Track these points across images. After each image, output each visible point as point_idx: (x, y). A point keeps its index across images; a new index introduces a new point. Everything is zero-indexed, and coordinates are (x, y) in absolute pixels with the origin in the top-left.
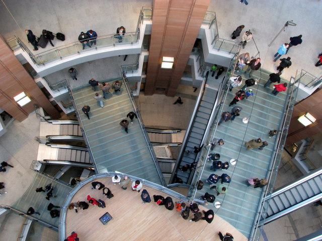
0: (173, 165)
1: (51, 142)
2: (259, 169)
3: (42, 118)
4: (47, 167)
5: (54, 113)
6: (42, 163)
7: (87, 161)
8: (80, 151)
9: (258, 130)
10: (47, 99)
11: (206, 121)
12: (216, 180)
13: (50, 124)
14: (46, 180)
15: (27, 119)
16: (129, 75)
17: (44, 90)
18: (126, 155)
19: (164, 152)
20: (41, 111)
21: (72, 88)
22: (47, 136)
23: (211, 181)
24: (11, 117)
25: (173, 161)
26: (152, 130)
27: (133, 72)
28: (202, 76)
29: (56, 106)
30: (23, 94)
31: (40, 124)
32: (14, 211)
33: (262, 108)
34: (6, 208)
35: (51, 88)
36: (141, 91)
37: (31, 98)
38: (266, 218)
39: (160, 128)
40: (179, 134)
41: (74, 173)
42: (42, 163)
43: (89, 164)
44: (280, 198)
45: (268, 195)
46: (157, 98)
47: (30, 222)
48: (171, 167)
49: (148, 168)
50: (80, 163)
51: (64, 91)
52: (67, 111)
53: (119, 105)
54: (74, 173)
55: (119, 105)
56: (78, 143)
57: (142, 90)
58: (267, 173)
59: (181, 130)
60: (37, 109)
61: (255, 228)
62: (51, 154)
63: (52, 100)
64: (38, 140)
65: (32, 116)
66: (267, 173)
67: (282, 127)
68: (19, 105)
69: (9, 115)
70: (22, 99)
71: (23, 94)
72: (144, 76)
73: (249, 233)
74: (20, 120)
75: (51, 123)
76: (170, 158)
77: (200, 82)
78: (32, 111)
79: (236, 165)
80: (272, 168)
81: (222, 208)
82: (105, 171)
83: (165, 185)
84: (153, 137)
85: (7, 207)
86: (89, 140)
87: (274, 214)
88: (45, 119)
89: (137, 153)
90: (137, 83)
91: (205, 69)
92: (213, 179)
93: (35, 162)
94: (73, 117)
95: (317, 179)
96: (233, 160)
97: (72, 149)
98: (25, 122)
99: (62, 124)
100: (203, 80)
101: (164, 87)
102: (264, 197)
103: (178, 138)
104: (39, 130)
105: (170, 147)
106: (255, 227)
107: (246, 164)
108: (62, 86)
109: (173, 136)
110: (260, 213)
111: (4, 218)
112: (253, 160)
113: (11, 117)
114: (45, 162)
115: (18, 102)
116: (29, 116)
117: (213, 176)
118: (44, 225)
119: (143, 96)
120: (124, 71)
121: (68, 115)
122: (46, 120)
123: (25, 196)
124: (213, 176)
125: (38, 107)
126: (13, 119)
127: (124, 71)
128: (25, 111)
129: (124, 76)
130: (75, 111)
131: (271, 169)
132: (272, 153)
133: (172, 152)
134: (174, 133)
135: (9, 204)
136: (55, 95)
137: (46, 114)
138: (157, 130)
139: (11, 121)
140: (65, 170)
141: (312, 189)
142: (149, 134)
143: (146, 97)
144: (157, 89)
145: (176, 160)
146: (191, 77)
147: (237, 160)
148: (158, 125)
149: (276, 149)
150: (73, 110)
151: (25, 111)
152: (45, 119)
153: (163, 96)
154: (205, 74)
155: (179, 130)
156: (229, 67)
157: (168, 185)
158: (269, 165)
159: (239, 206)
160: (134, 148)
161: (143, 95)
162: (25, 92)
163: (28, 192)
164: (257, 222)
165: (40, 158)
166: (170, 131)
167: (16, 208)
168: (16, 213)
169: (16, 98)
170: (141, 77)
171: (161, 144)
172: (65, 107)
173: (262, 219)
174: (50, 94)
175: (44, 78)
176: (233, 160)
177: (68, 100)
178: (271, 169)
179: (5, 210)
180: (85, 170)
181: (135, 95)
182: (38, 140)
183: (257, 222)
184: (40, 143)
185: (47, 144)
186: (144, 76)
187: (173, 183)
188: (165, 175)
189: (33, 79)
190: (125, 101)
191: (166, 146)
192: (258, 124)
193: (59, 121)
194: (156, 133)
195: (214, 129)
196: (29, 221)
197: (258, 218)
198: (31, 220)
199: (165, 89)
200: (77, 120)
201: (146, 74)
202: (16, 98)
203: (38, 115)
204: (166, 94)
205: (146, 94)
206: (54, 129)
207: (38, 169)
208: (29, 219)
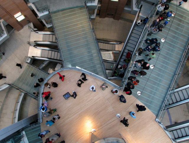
0: (115, 64)
1: (37, 45)
2: (163, 85)
3: (32, 29)
4: (35, 61)
5: (40, 26)
6: (31, 58)
7: (58, 59)
8: (57, 52)
9: (171, 47)
10: (35, 17)
11: (140, 33)
12: (150, 49)
13: (37, 34)
14: (33, 69)
15: (22, 30)
16: (89, 4)
17: (33, 11)
18: (84, 57)
19: (108, 56)
20: (31, 25)
21: (51, 10)
22: (35, 41)
23: (147, 50)
24: (13, 28)
25: (115, 62)
26: (103, 41)
27: (91, 2)
28: (138, 8)
29: (42, 22)
30: (20, 14)
31: (30, 33)
32: (14, 87)
33: (175, 33)
34: (8, 84)
35: (38, 10)
36: (97, 15)
37: (25, 16)
38: (169, 105)
39: (108, 40)
40: (120, 45)
41: (53, 64)
42: (31, 58)
43: (60, 60)
44: (178, 93)
45: (172, 90)
46: (108, 20)
47: (23, 94)
48: (113, 66)
49: (97, 66)
50: (57, 60)
51: (46, 13)
52: (48, 26)
53: (81, 23)
54: (53, 64)
55: (81, 23)
56: (54, 47)
57: (98, 14)
58: (174, 76)
59: (122, 43)
60: (29, 23)
61: (161, 111)
62: (36, 53)
63: (39, 18)
64: (29, 43)
65: (26, 28)
66: (174, 76)
67: (188, 47)
68: (17, 21)
69: (11, 27)
70: (20, 17)
71: (20, 14)
72: (99, 5)
73: (157, 113)
74: (18, 30)
75: (38, 33)
76: (113, 60)
77: (136, 12)
78: (26, 25)
79: (153, 69)
80: (177, 73)
81: (142, 96)
82: (70, 66)
83: (107, 78)
84: (102, 45)
85: (9, 84)
86: (62, 45)
87: (173, 103)
88: (34, 30)
89: (92, 55)
90: (94, 10)
91: (140, 3)
92: (149, 49)
93: (27, 57)
94: (52, 30)
95: (186, 129)
96: (152, 65)
97: (49, 50)
98: (22, 31)
99: (44, 34)
100: (138, 10)
101: (112, 13)
102: (170, 91)
103: (119, 48)
104: (30, 37)
105: (113, 53)
106: (168, 94)
107: (160, 69)
108: (44, 10)
109: (117, 46)
110: (167, 98)
111: (7, 91)
112: (164, 71)
113: (13, 28)
114: (33, 58)
115: (17, 19)
116: (24, 28)
117: (149, 47)
118: (32, 97)
119: (98, 19)
120: (85, 2)
121: (49, 28)
122: (35, 31)
123: (20, 78)
124: (149, 47)
125: (30, 22)
126: (14, 29)
127: (85, 2)
128: (21, 24)
129: (86, 5)
130: (52, 26)
131: (171, 87)
132: (184, 50)
133: (115, 57)
134: (117, 44)
135: (11, 82)
136: (40, 15)
137: (35, 27)
138: (106, 41)
139: (12, 31)
140: (46, 63)
141: (181, 132)
142: (99, 43)
143: (101, 19)
144: (108, 14)
145: (116, 62)
146: (131, 8)
147: (154, 66)
148: (107, 38)
149: (181, 61)
150: (51, 25)
151: (21, 24)
152: (34, 30)
153: (112, 19)
154: (140, 7)
155: (121, 42)
156: (155, 3)
157: (109, 78)
158: (181, 58)
159: (152, 95)
160: (89, 52)
161: (99, 18)
162: (21, 12)
163: (22, 76)
164: (163, 107)
165: (30, 55)
166: (115, 43)
167: (15, 85)
168: (15, 88)
169: (16, 16)
170: (97, 6)
171: (108, 51)
172: (47, 23)
173: (166, 106)
174: (37, 15)
175: (33, 3)
176: (152, 65)
177: (49, 18)
178: (171, 87)
179: (8, 86)
180: (58, 64)
181: (92, 17)
182: (29, 43)
183: (163, 107)
184: (30, 45)
185: (34, 46)
186: (99, 5)
187: (112, 77)
188: (107, 71)
189: (27, 3)
190: (84, 22)
191: (111, 52)
192: (171, 43)
193: (43, 32)
194: (106, 43)
195: (141, 44)
196: (23, 93)
197: (164, 105)
198: (24, 93)
199: (113, 15)
200: (53, 32)
201: (101, 4)
202: (16, 16)
203: (30, 27)
204: (114, 18)
205: (100, 17)
206: (40, 36)
207: (29, 61)
208: (22, 92)
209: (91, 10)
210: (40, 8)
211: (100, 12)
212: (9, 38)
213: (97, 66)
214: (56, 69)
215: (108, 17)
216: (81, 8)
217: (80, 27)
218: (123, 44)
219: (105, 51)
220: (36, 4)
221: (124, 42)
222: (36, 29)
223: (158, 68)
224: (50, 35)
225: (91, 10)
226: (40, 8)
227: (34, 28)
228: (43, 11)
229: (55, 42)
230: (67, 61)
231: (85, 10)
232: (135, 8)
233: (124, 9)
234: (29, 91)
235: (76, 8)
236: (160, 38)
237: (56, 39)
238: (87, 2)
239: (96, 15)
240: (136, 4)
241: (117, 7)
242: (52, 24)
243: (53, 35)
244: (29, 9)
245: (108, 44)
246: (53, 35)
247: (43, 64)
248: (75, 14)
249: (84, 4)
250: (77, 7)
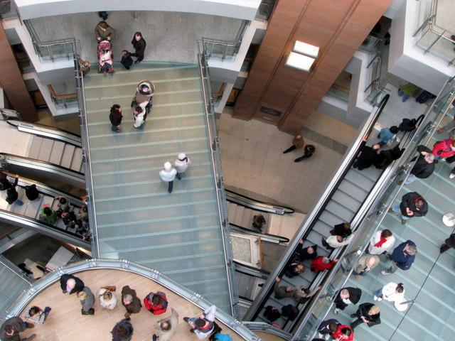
13: (14, 130)
16: (213, 63)
17: (18, 49)
19: (248, 250)
27: (223, 58)
28: (373, 103)
35: (38, 50)
52: (56, 111)
59: (293, 210)
63: (29, 76)
75: (16, 127)
76: (255, 266)
77: (364, 115)
100: (373, 111)
103: (283, 227)
108: (61, 52)
119: (228, 118)
122: (7, 118)
127: (205, 53)
133: (263, 255)
136: (41, 66)
140: (20, 238)
143: (236, 121)
144: (263, 109)
152: (4, 116)
154: (379, 100)
180: (62, 249)
193: (35, 127)
199: (279, 114)
202: (299, 45)
205: (235, 115)
209: (215, 83)
210: (47, 42)
211: (235, 101)
212: (51, 114)
213: (208, 275)
214: (49, 265)
215: (260, 118)
216: (185, 70)
217: (172, 132)
218: (298, 217)
219: (243, 233)
220: (36, 28)
221: (307, 213)
222: (9, 113)
223: (423, 313)
224: (56, 142)
225: (215, 83)
226: (47, 42)
227: (5, 108)
228: (54, 56)
229: (79, 173)
230: (108, 243)
231: (198, 78)
232: (362, 102)
233: (321, 101)
234: (333, 200)
235: (169, 66)
236: (443, 213)
237: (85, 160)
238: (210, 56)
239: (226, 105)
240: (370, 89)
241: (300, 88)
242: (81, 105)
243: (66, 143)
244: (6, 38)
245: (246, 207)
246: (66, 143)
247: (10, 239)
248: (207, 87)
249: (196, 60)
250: (173, 65)
